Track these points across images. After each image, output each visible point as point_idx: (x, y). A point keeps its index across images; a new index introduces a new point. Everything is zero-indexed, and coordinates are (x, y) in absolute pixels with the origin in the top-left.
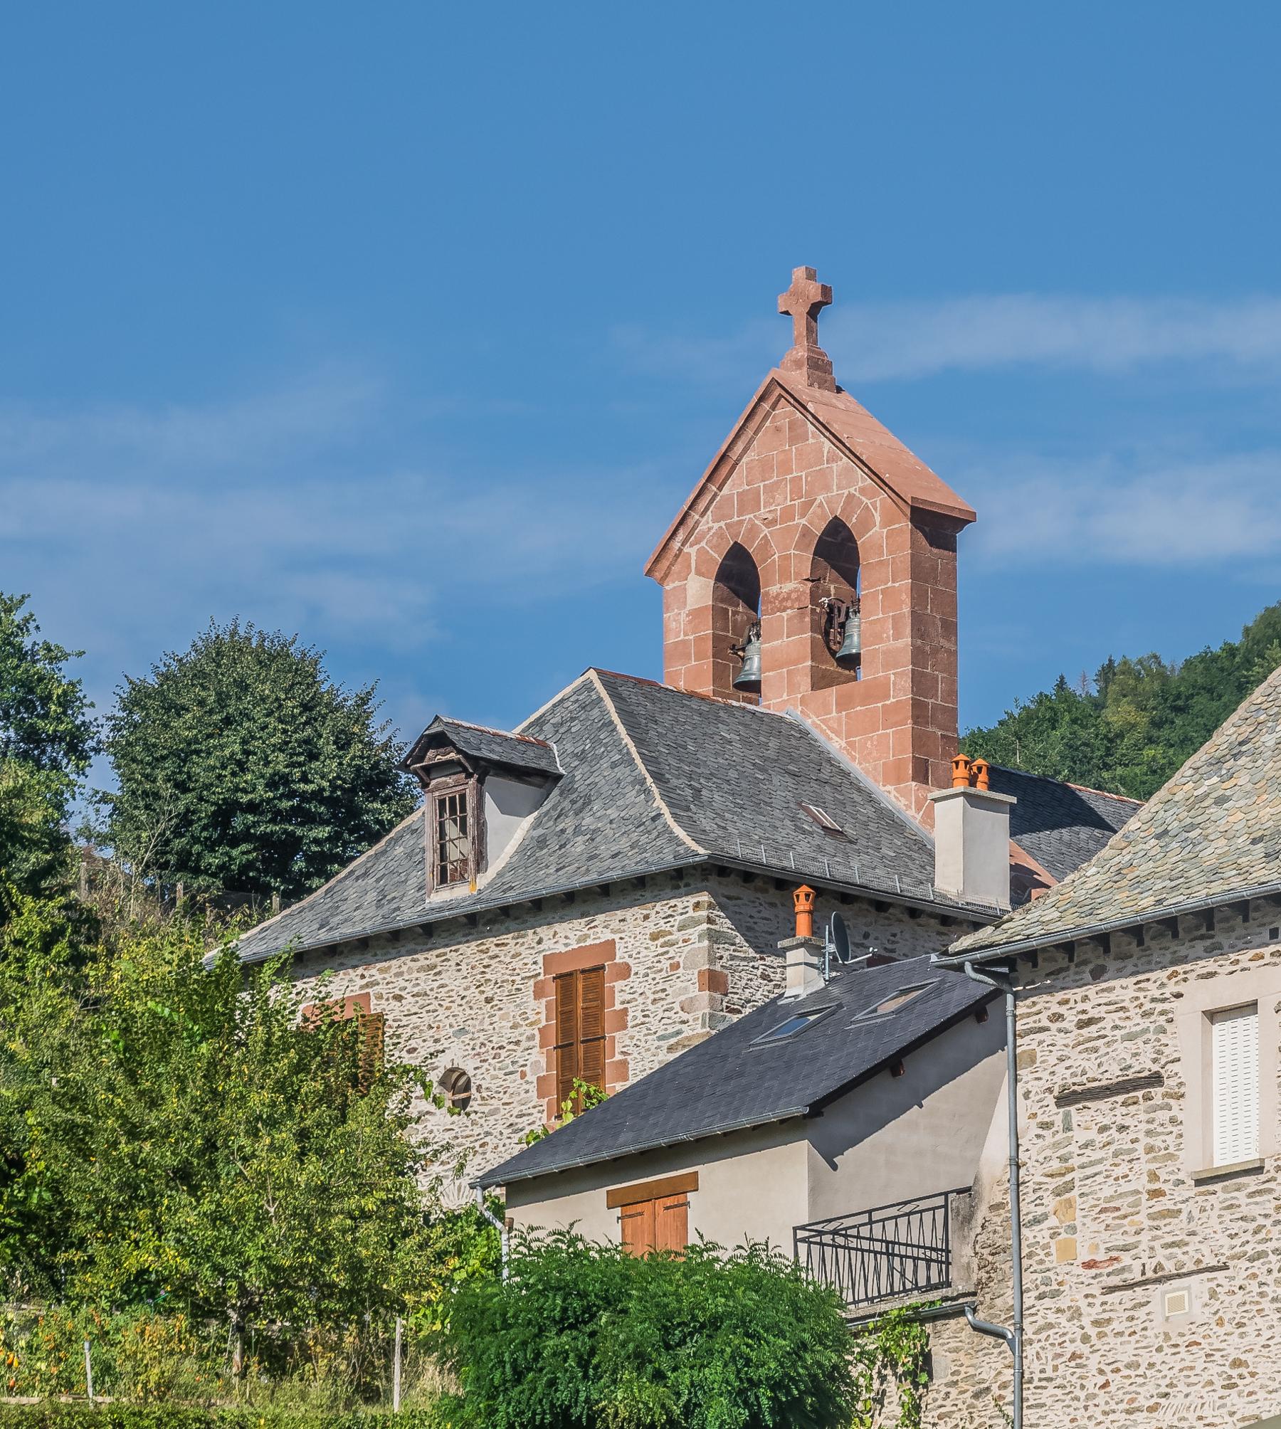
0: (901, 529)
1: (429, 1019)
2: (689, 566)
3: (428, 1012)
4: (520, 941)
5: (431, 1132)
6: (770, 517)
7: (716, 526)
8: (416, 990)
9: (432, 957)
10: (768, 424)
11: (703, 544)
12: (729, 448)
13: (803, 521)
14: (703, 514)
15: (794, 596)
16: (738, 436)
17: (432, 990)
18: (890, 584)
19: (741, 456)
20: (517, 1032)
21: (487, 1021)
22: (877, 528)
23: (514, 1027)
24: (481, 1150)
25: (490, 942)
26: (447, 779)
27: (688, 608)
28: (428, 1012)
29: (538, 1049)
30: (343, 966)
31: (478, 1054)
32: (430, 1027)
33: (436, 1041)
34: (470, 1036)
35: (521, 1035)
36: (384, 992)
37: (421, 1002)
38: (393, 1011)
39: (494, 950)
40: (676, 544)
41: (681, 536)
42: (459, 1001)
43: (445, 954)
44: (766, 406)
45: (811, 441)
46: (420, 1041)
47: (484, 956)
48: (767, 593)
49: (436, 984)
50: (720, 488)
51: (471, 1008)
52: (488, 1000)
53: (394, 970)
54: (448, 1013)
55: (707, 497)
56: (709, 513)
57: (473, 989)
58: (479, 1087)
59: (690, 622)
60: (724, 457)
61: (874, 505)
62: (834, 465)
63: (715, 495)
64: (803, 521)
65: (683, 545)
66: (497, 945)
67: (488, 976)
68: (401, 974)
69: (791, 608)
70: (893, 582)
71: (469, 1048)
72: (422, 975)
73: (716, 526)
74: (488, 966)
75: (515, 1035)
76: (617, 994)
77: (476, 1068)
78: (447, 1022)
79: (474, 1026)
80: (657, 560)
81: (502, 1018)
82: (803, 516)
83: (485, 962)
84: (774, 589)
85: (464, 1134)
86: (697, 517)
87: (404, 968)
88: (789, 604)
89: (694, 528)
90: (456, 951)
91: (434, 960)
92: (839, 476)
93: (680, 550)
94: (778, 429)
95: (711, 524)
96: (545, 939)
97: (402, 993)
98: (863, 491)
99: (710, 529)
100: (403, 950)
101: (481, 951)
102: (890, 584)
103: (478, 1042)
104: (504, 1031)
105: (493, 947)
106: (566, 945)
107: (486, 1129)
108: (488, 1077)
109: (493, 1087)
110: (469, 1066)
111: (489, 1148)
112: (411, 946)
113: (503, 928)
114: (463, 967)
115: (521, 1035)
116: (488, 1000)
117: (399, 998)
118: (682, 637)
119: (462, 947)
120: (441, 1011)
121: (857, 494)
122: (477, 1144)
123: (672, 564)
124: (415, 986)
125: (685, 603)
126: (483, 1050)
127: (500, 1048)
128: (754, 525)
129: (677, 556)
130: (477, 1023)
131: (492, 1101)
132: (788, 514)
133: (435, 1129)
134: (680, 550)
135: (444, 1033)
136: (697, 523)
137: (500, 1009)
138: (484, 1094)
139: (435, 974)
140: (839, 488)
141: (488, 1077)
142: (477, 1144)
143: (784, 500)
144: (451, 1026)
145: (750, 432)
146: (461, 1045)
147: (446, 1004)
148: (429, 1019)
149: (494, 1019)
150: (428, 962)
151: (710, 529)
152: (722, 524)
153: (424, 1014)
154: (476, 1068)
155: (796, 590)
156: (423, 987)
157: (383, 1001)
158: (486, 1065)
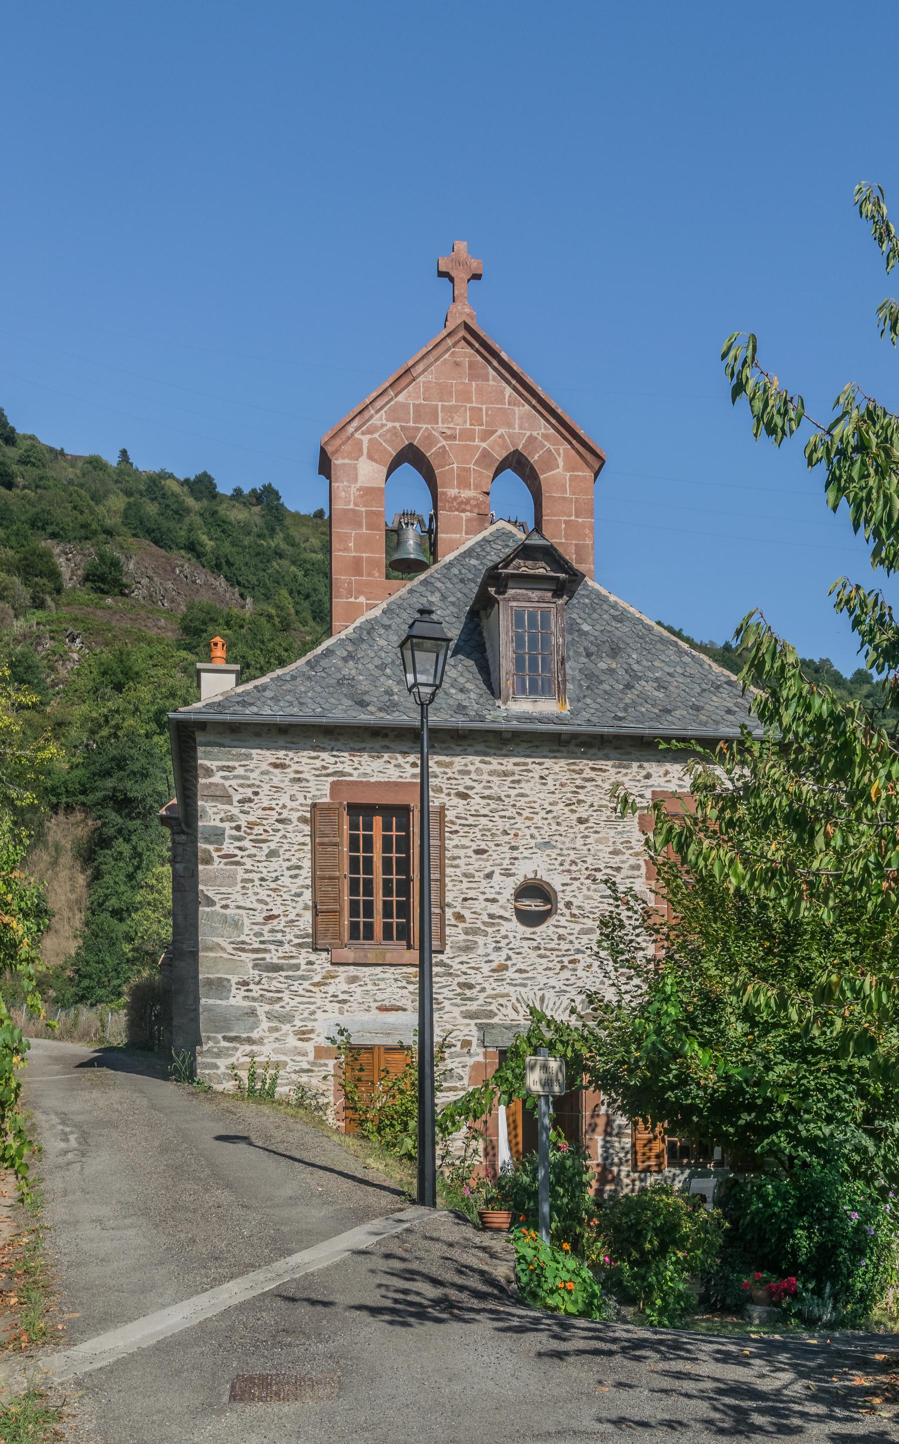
0: (584, 477)
1: (501, 824)
2: (361, 450)
3: (501, 817)
4: (624, 771)
5: (506, 937)
6: (449, 432)
7: (390, 425)
8: (487, 792)
9: (509, 763)
10: (446, 356)
11: (376, 435)
12: (413, 366)
13: (484, 445)
14: (377, 412)
15: (472, 502)
16: (423, 358)
17: (508, 796)
18: (573, 518)
19: (420, 375)
20: (617, 858)
21: (582, 841)
22: (560, 470)
23: (615, 852)
24: (570, 966)
25: (585, 764)
26: (530, 593)
27: (359, 484)
28: (501, 817)
29: (643, 880)
30: (387, 749)
31: (569, 871)
32: (506, 833)
33: (513, 848)
34: (559, 851)
35: (623, 862)
36: (444, 786)
37: (493, 806)
38: (455, 809)
39: (588, 773)
40: (350, 429)
41: (355, 424)
42: (543, 814)
43: (525, 764)
44: (450, 342)
45: (491, 383)
46: (491, 844)
47: (577, 776)
48: (445, 493)
49: (513, 792)
50: (396, 395)
51: (558, 824)
52: (581, 821)
53: (457, 767)
54: (528, 823)
55: (385, 399)
56: (383, 412)
57: (561, 806)
58: (568, 905)
59: (361, 496)
60: (408, 370)
61: (557, 451)
62: (516, 409)
63: (391, 400)
64: (484, 445)
65: (356, 431)
66: (593, 769)
67: (581, 797)
68: (468, 773)
69: (471, 511)
70: (577, 516)
71: (557, 863)
72: (495, 779)
73: (390, 425)
74: (583, 787)
75: (615, 861)
76: (328, 792)
77: (563, 885)
78: (528, 832)
79: (564, 843)
80: (333, 437)
81: (598, 841)
82: (483, 440)
83: (579, 782)
84: (452, 492)
85: (549, 946)
86: (372, 412)
87: (471, 768)
88: (468, 507)
89: (368, 420)
90: (540, 764)
91: (510, 767)
92: (521, 418)
93: (352, 434)
94: (457, 364)
95: (384, 422)
96: (654, 775)
97: (469, 792)
98: (545, 436)
99: (383, 425)
100: (470, 749)
101: (573, 771)
102: (573, 518)
103: (568, 859)
104: (601, 855)
105: (588, 770)
106: (680, 786)
107: (577, 946)
108: (580, 896)
109: (587, 908)
110: (556, 881)
111: (580, 966)
112: (481, 747)
113: (600, 754)
114: (550, 780)
115: (623, 862)
116: (581, 821)
117: (464, 796)
118: (352, 506)
119: (548, 762)
120: (518, 819)
121: (540, 438)
122: (566, 960)
123: (343, 444)
124: (485, 788)
125: (356, 480)
126: (574, 868)
127: (596, 870)
128: (430, 434)
129: (349, 438)
130: (567, 840)
131: (585, 920)
132: (468, 435)
133: (511, 935)
134: (352, 434)
135: (524, 842)
136: (371, 417)
137: (596, 832)
138: (575, 911)
139: (513, 782)
140: (521, 428)
141: (580, 896)
142: (566, 960)
143: (461, 422)
144: (532, 836)
145: (431, 358)
146: (547, 859)
147: (526, 813)
148: (501, 824)
149: (589, 841)
150: (503, 768)
151: (383, 425)
152: (397, 425)
153: (497, 819)
154: (563, 885)
155: (475, 498)
156: (495, 791)
157: (443, 795)
158: (577, 884)
